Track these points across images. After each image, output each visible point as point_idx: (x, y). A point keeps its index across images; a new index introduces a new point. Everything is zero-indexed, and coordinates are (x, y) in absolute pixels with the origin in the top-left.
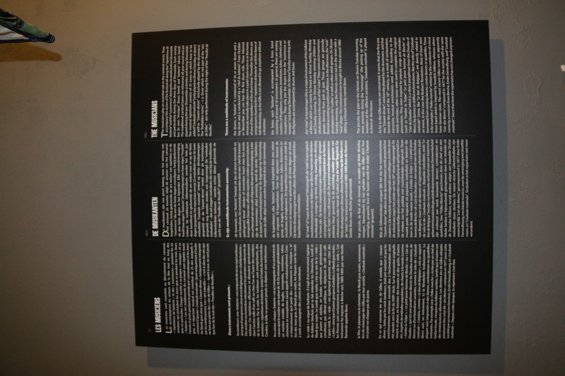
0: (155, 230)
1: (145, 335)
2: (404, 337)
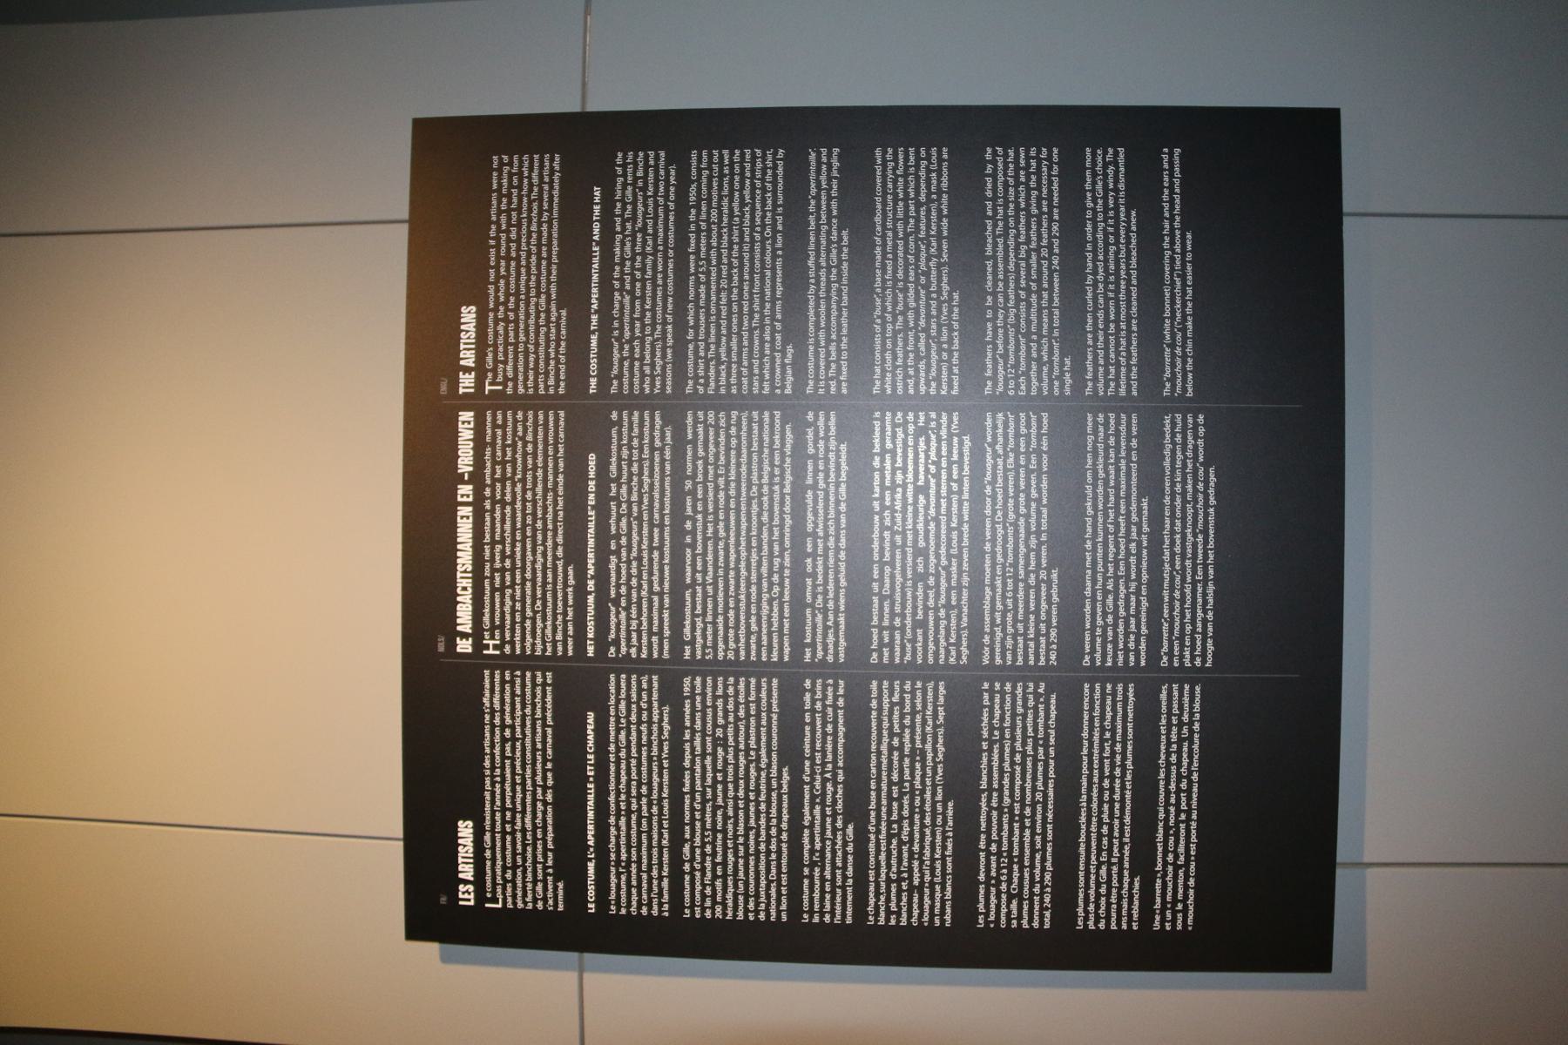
0: (464, 636)
1: (433, 912)
2: (987, 922)
